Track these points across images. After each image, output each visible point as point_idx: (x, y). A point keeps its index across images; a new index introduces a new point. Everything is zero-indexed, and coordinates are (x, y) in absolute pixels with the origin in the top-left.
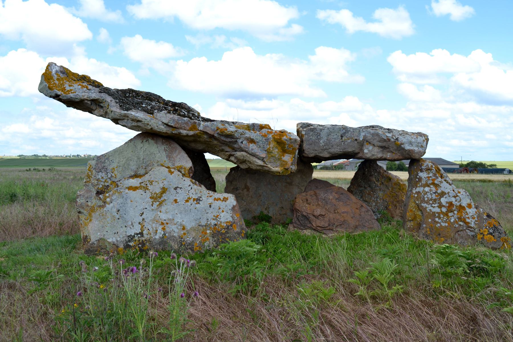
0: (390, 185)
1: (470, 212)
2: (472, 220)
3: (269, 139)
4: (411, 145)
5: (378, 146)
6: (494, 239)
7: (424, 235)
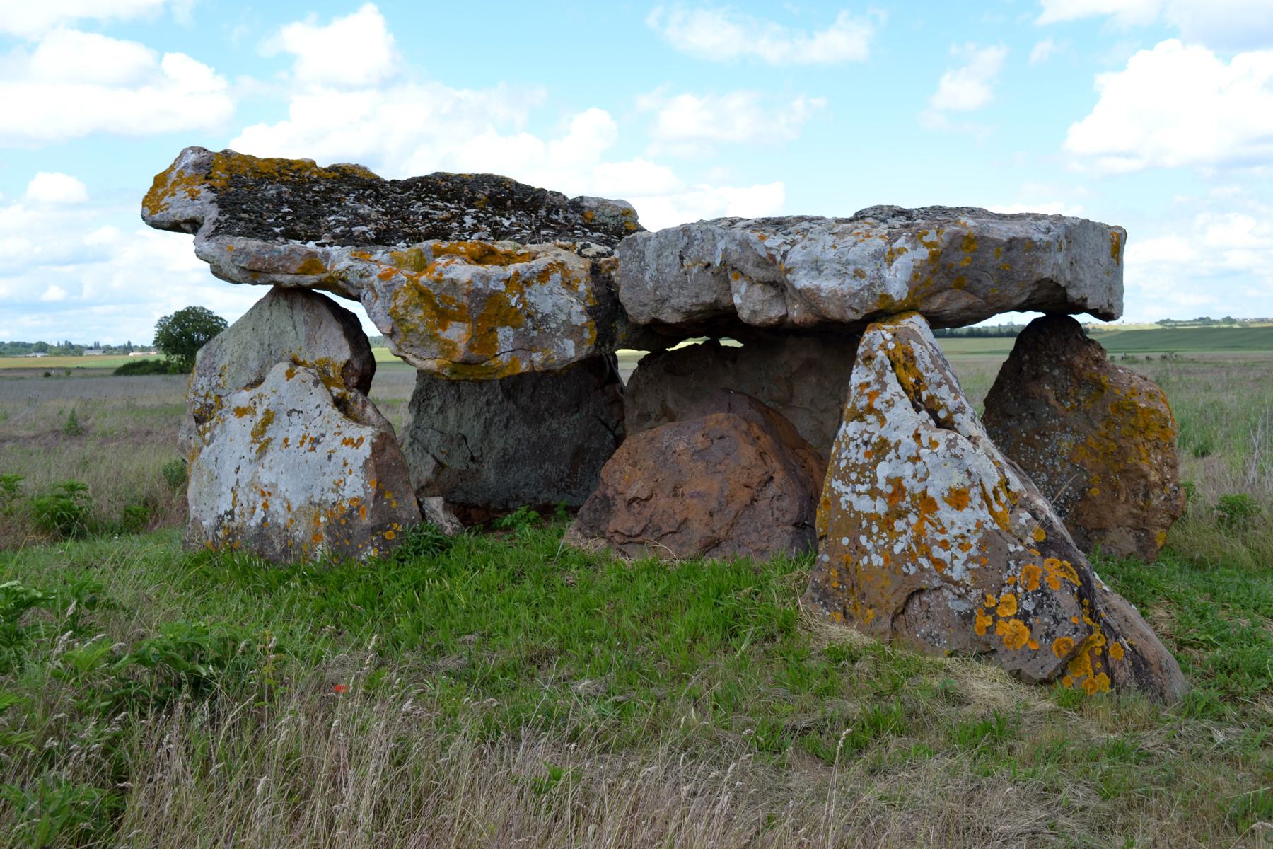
0: (1100, 412)
1: (953, 523)
2: (959, 553)
3: (394, 284)
4: (814, 273)
5: (759, 282)
6: (1031, 639)
7: (815, 590)
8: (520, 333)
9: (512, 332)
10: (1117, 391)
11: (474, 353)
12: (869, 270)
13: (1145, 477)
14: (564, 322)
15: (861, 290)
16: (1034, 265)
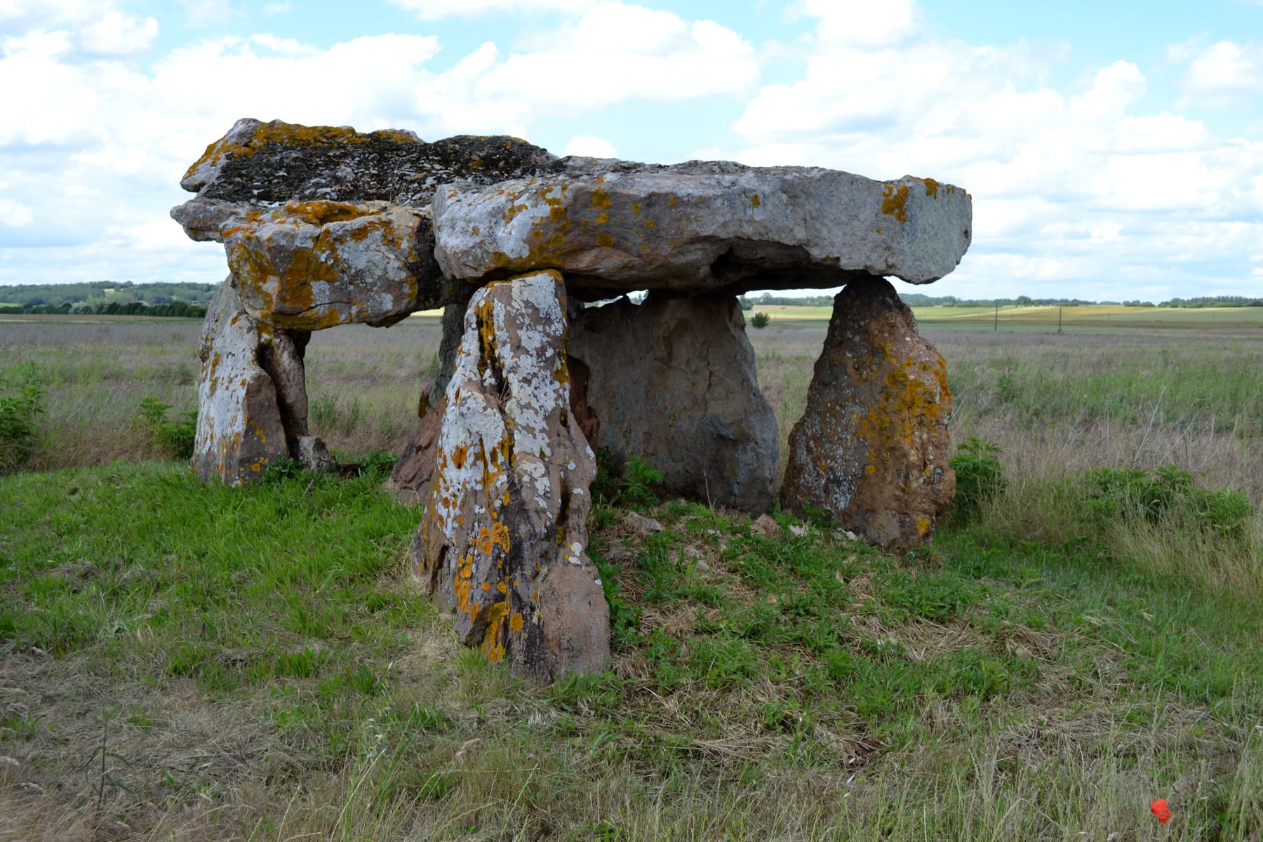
8: (336, 287)
9: (327, 286)
10: (894, 361)
11: (287, 304)
12: (483, 228)
13: (905, 456)
14: (380, 277)
15: (473, 247)
16: (684, 222)
